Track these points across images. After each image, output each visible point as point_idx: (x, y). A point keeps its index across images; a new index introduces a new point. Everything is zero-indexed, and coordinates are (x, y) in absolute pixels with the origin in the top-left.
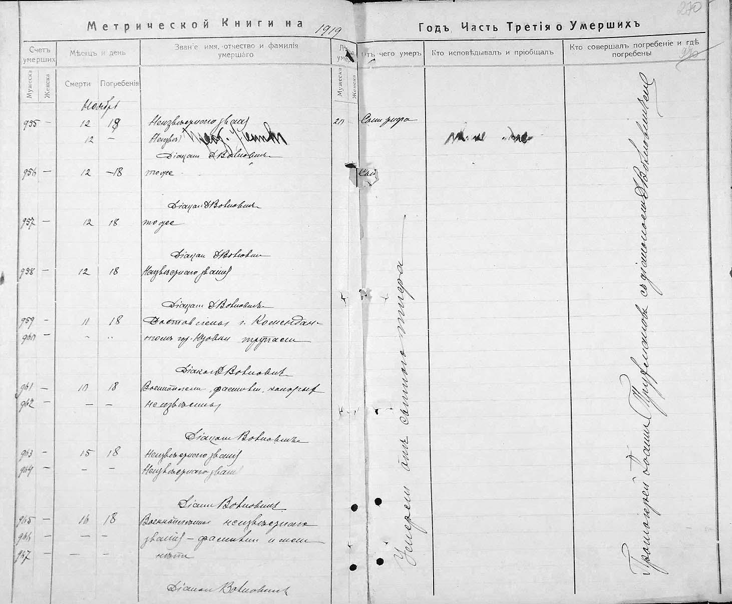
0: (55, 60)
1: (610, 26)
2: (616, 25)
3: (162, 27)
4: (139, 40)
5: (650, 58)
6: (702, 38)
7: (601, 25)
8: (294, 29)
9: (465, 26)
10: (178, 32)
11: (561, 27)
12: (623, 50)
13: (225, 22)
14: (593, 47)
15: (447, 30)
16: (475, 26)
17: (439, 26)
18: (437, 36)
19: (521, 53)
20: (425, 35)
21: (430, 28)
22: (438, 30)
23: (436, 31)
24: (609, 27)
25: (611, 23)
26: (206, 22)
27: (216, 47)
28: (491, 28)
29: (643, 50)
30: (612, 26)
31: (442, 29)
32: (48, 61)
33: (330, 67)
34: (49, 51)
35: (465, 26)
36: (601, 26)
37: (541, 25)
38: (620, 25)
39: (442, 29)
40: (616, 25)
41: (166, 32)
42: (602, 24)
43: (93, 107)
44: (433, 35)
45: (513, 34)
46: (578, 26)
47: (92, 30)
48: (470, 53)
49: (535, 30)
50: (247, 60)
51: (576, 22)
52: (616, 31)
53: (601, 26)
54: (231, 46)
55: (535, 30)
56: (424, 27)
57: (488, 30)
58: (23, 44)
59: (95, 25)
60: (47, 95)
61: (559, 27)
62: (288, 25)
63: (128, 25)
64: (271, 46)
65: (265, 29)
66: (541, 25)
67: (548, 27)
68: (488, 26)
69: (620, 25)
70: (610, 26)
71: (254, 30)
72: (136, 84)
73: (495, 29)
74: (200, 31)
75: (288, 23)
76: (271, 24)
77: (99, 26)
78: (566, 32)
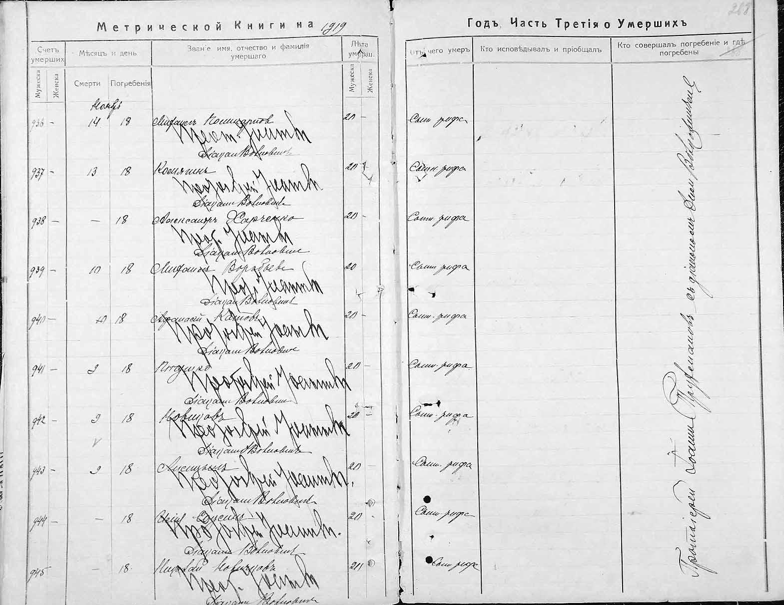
0: (64, 60)
1: (658, 25)
2: (663, 24)
3: (174, 29)
4: (150, 41)
5: (697, 57)
6: (748, 38)
7: (648, 24)
8: (305, 30)
9: (514, 22)
10: (190, 34)
11: (609, 25)
12: (672, 49)
13: (237, 25)
14: (641, 46)
15: (496, 25)
16: (524, 22)
17: (488, 21)
18: (487, 31)
19: (568, 50)
20: (474, 30)
21: (479, 23)
22: (487, 25)
23: (485, 26)
24: (656, 25)
25: (658, 22)
26: (219, 25)
27: (229, 49)
28: (540, 24)
29: (690, 48)
30: (659, 25)
31: (491, 24)
32: (57, 61)
33: (342, 64)
34: (57, 51)
35: (514, 22)
36: (648, 24)
37: (589, 23)
38: (667, 24)
39: (491, 24)
40: (663, 24)
41: (179, 33)
42: (650, 23)
43: (101, 107)
44: (482, 31)
45: (561, 31)
46: (625, 24)
47: (101, 31)
48: (519, 49)
49: (583, 27)
50: (261, 61)
51: (623, 20)
52: (663, 30)
53: (648, 24)
54: (244, 48)
55: (583, 27)
56: (473, 22)
57: (537, 26)
58: (31, 44)
59: (105, 26)
60: (56, 95)
61: (607, 25)
62: (299, 26)
63: (138, 26)
64: (283, 47)
65: (276, 31)
66: (589, 23)
67: (596, 25)
68: (537, 22)
69: (667, 24)
70: (658, 25)
71: (266, 32)
72: (147, 85)
73: (544, 25)
74: (213, 33)
75: (299, 25)
76: (282, 26)
77: (110, 27)
78: (614, 30)
